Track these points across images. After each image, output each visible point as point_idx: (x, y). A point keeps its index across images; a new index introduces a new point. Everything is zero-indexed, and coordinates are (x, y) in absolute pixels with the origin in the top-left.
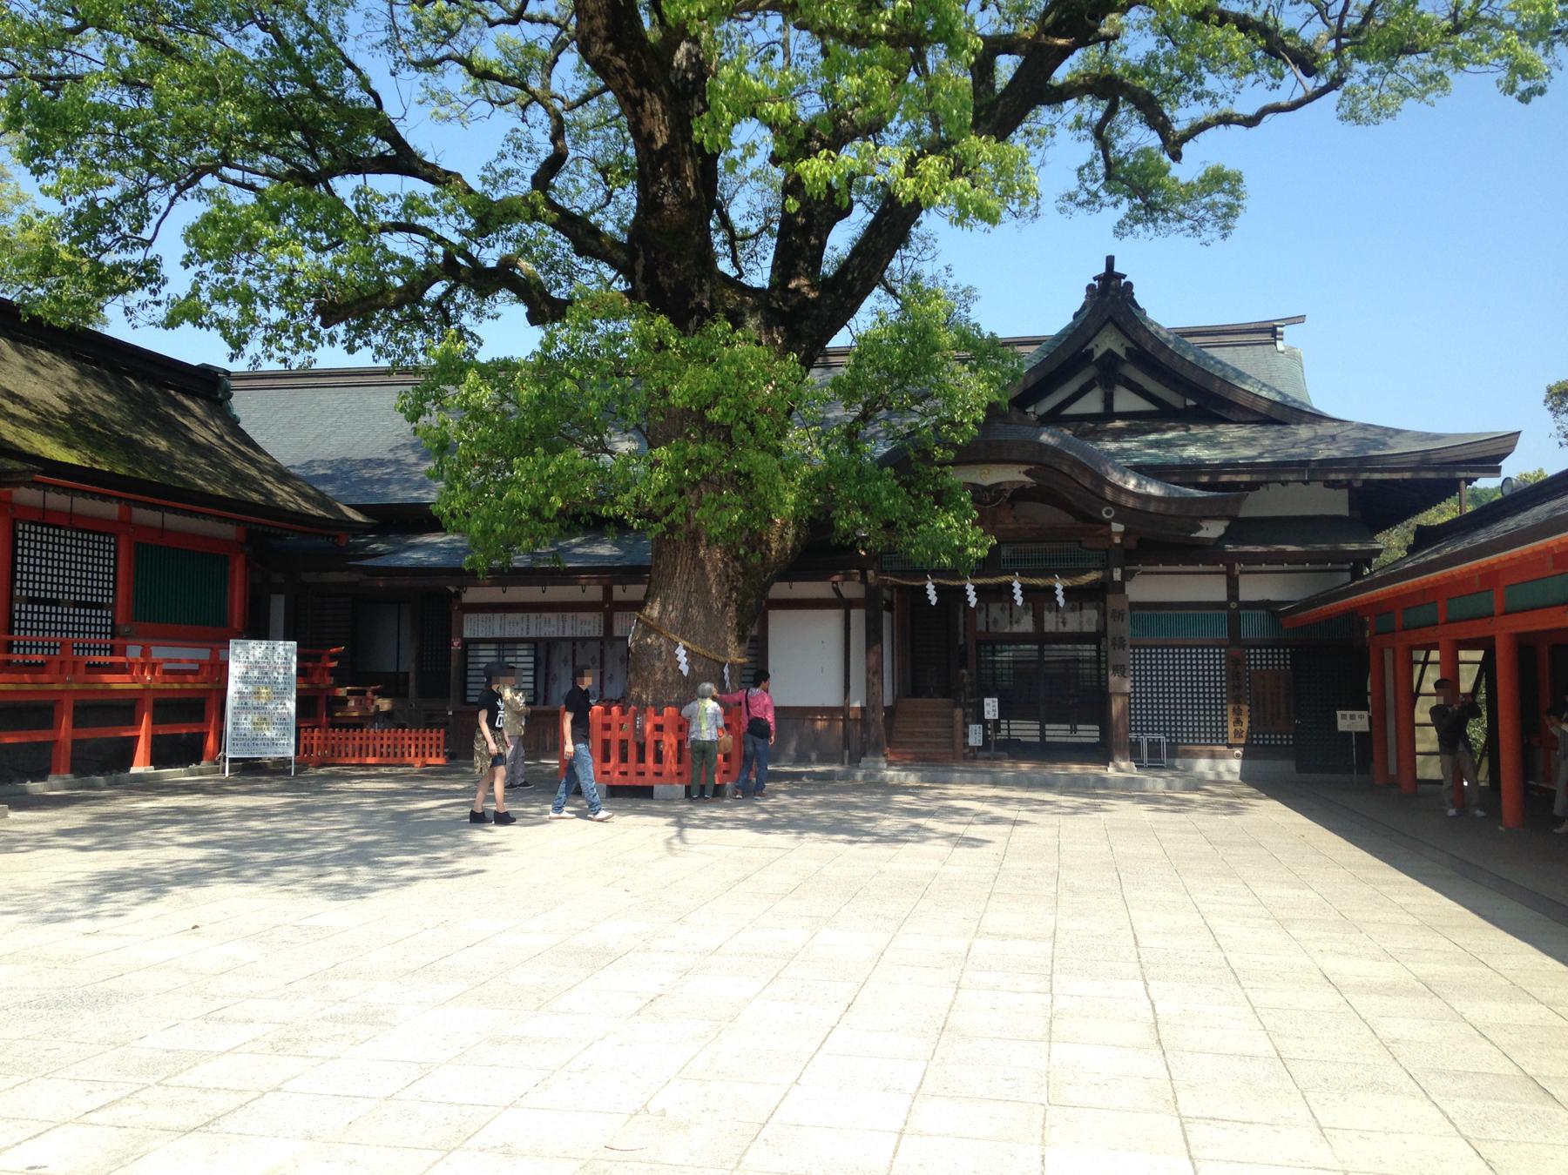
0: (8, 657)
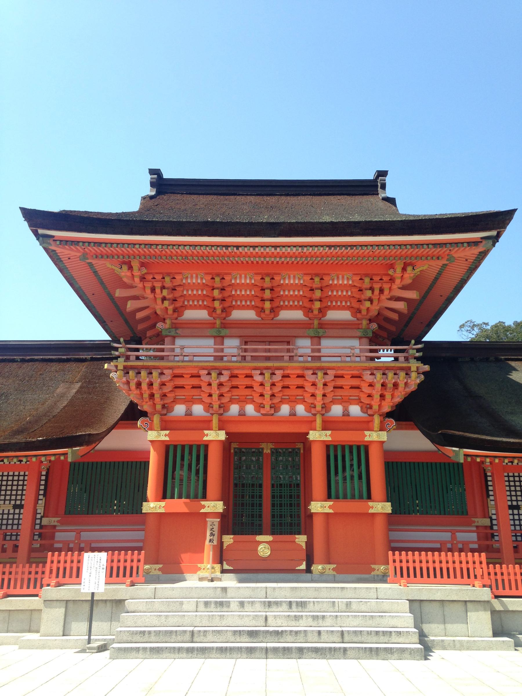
0: (41, 531)
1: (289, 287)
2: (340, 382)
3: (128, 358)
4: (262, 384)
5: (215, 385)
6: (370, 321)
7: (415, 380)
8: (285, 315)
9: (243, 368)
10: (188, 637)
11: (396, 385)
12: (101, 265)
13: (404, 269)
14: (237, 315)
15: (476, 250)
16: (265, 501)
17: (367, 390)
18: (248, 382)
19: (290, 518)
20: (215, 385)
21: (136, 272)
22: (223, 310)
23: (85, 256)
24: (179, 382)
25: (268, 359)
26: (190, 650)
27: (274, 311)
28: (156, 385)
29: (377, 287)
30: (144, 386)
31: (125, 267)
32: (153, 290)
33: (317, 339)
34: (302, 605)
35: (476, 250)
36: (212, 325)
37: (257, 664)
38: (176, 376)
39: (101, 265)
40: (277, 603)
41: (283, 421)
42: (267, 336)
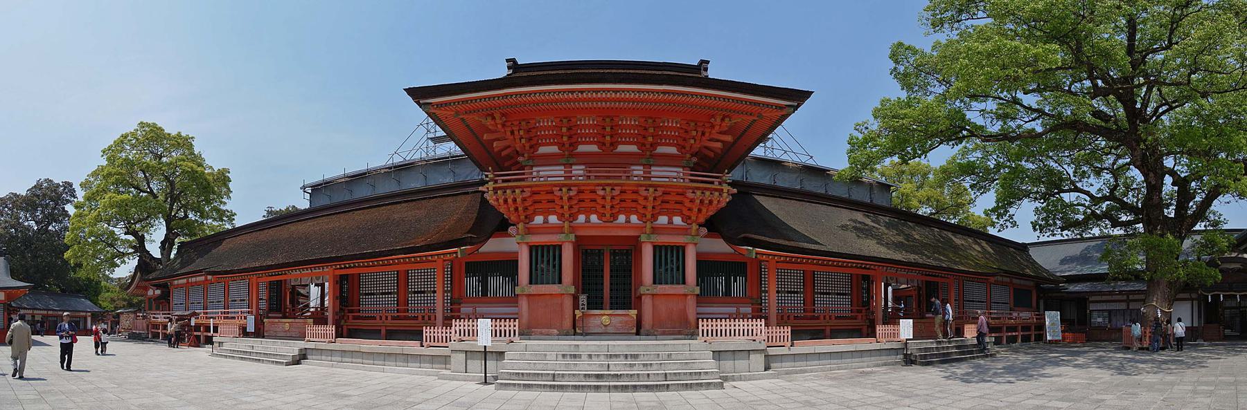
1: (626, 127)
2: (667, 198)
3: (496, 182)
4: (604, 198)
5: (565, 198)
6: (692, 155)
7: (726, 198)
8: (622, 148)
9: (589, 185)
10: (550, 378)
11: (711, 202)
12: (471, 118)
13: (723, 120)
14: (582, 148)
15: (780, 113)
16: (606, 283)
17: (688, 204)
18: (592, 196)
19: (625, 298)
20: (565, 198)
21: (498, 121)
22: (571, 144)
23: (457, 113)
24: (537, 197)
25: (608, 178)
26: (554, 386)
27: (614, 144)
28: (519, 200)
29: (700, 130)
30: (510, 201)
31: (489, 119)
32: (512, 133)
33: (648, 166)
34: (635, 357)
35: (780, 113)
36: (562, 156)
37: (603, 396)
38: (534, 193)
39: (471, 118)
40: (616, 356)
41: (620, 227)
42: (607, 160)
